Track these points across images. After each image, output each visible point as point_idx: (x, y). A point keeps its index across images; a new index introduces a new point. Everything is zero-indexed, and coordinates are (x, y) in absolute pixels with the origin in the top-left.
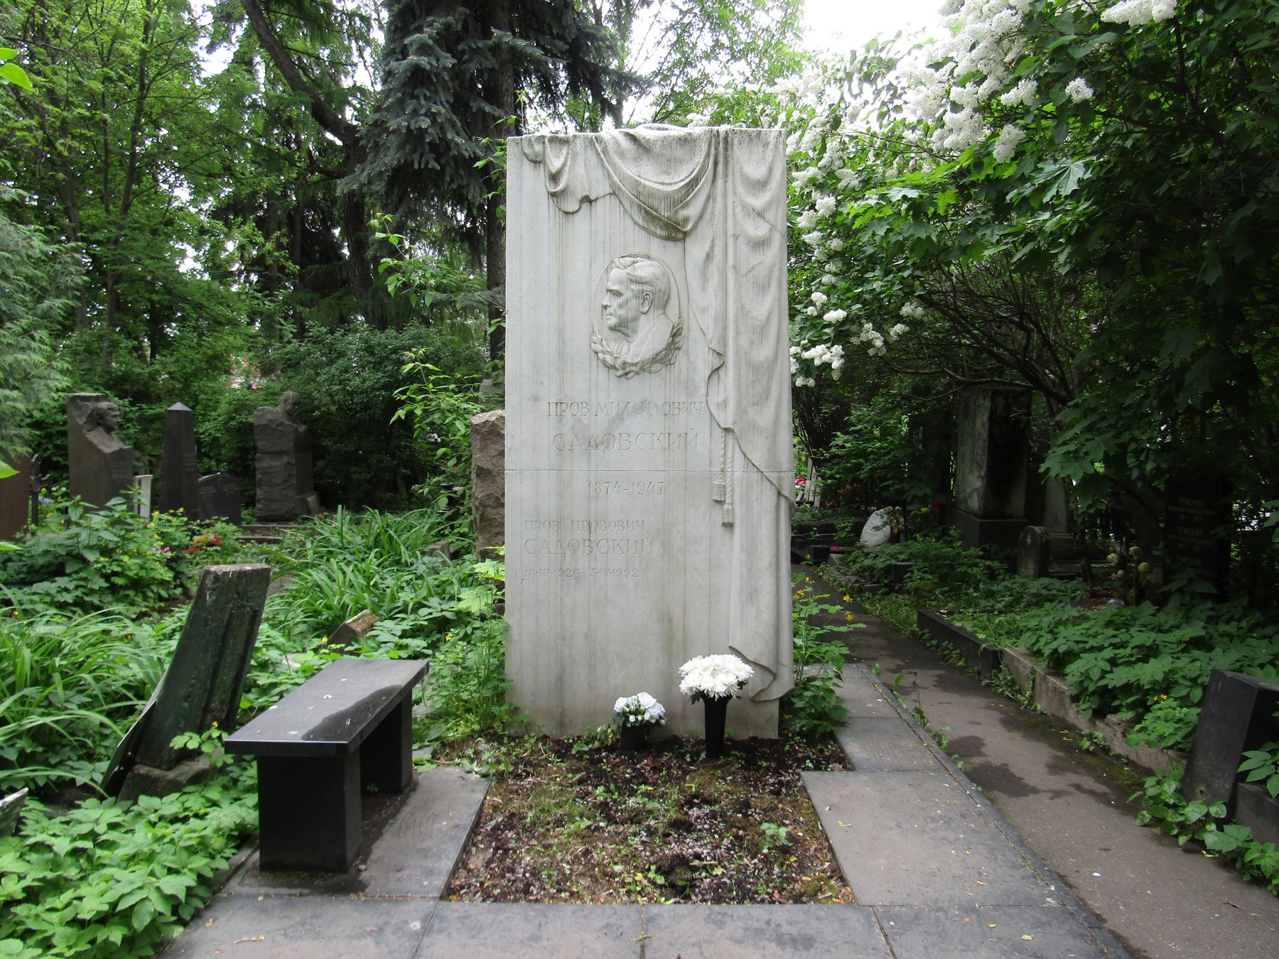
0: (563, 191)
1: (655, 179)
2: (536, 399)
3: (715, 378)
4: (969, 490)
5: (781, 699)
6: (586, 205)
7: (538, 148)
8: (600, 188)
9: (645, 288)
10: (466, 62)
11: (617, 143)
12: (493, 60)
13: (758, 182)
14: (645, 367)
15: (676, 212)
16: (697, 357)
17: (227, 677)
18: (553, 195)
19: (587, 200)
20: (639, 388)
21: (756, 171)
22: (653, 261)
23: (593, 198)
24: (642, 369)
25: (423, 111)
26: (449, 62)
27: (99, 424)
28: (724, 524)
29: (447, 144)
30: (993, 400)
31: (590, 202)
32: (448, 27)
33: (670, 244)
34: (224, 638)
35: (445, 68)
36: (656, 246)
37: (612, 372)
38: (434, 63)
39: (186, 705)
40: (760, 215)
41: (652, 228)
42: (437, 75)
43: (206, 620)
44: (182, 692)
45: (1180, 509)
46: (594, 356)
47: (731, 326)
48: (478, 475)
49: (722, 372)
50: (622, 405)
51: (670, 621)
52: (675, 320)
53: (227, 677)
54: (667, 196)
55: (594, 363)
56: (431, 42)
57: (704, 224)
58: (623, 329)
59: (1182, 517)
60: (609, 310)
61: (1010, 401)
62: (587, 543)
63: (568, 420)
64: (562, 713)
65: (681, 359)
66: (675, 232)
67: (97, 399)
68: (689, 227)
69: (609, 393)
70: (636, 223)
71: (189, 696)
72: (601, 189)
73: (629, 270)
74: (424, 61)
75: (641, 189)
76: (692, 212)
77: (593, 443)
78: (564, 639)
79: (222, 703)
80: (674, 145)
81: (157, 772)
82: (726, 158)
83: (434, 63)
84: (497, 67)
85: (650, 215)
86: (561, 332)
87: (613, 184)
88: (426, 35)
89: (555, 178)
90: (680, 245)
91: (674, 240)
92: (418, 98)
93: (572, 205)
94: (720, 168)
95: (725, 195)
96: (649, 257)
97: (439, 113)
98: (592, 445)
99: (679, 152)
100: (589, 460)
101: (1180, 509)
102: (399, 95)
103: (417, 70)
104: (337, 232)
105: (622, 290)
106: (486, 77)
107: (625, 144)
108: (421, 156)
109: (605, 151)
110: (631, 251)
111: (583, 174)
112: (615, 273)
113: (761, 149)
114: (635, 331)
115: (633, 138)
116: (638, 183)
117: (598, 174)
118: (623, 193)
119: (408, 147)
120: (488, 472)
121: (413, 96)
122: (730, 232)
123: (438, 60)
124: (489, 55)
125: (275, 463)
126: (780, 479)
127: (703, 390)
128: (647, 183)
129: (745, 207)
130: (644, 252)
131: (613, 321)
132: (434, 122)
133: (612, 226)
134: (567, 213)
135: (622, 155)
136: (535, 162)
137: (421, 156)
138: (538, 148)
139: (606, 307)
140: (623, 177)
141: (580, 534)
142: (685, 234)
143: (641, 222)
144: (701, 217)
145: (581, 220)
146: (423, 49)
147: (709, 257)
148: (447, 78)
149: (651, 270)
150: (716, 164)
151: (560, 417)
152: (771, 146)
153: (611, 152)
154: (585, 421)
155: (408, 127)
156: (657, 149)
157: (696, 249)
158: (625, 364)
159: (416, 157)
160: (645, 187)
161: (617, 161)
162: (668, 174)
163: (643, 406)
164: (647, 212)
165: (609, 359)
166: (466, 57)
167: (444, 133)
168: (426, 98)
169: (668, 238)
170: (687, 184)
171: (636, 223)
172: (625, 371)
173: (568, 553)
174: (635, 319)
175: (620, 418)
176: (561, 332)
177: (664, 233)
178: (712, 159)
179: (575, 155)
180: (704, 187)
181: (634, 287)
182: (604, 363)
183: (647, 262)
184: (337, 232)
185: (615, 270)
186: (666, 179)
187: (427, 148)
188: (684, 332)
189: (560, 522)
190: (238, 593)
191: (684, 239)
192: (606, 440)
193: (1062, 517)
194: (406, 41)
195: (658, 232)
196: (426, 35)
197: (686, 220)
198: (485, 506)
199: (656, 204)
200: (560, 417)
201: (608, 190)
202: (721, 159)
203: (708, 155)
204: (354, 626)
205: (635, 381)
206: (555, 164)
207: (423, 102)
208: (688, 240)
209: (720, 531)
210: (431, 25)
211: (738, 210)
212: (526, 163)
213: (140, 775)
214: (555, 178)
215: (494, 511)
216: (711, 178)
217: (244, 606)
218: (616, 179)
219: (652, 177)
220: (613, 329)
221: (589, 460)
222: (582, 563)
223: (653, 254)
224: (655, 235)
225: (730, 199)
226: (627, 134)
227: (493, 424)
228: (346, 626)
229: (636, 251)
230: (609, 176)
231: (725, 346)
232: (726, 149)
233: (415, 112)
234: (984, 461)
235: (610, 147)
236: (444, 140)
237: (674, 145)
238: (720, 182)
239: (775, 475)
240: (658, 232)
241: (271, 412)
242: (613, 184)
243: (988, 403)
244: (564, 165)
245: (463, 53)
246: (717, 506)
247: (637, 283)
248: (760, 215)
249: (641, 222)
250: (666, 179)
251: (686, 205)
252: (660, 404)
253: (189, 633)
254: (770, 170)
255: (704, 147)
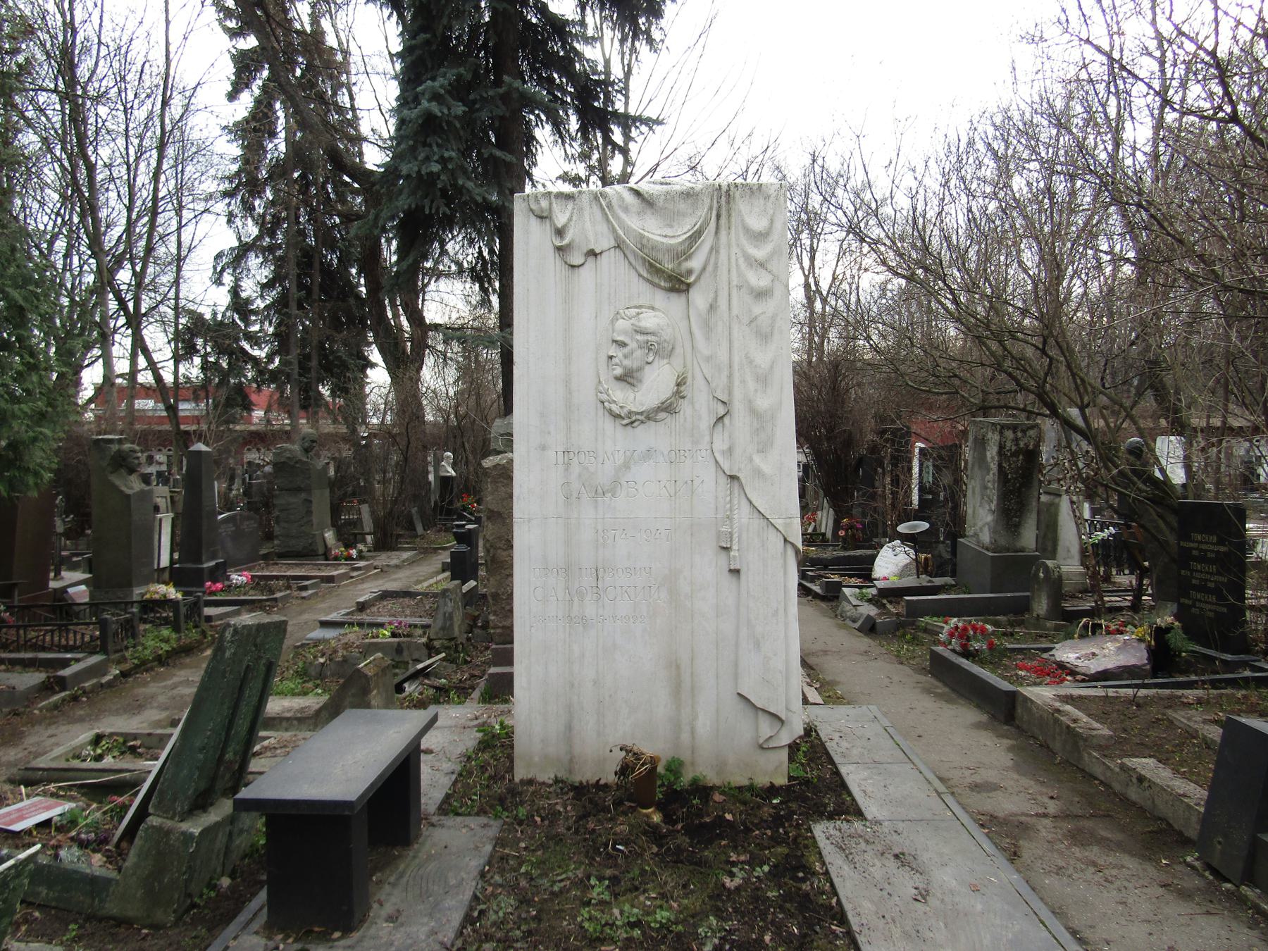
0: (569, 246)
1: (659, 232)
2: (543, 448)
3: (720, 425)
4: (980, 524)
5: (790, 746)
6: (591, 259)
7: (544, 204)
8: (603, 242)
9: (650, 338)
10: (478, 110)
11: (622, 199)
12: (504, 108)
13: (761, 234)
14: (649, 416)
15: (680, 264)
16: (699, 407)
17: (242, 725)
18: (559, 249)
19: (592, 254)
20: (646, 436)
21: (757, 223)
22: (662, 313)
23: (598, 251)
24: (648, 418)
25: (436, 158)
26: (459, 109)
27: (121, 466)
28: (731, 571)
29: (460, 190)
30: (1001, 433)
31: (595, 255)
32: (459, 76)
33: (674, 296)
34: (241, 689)
35: (456, 117)
36: (660, 298)
37: (618, 421)
38: (446, 111)
39: (201, 756)
40: (762, 265)
41: (657, 281)
42: (448, 123)
43: (225, 671)
44: (198, 743)
45: (1192, 545)
46: (600, 405)
47: (736, 375)
48: (489, 518)
49: (726, 420)
50: (628, 453)
51: (678, 667)
52: (680, 369)
53: (242, 725)
54: (669, 249)
55: (601, 412)
56: (442, 91)
57: (707, 274)
58: (628, 378)
59: (1195, 553)
60: (615, 360)
61: (1019, 434)
62: (595, 590)
63: (576, 469)
64: (571, 761)
65: (685, 407)
66: (678, 284)
67: (120, 441)
68: (692, 279)
69: (617, 441)
70: (640, 275)
71: (204, 748)
72: (603, 242)
73: (633, 321)
74: (435, 108)
75: (645, 241)
76: (695, 263)
77: (600, 491)
78: (573, 685)
79: (235, 754)
80: (677, 199)
81: (169, 823)
82: (729, 210)
83: (446, 111)
84: (507, 115)
85: (654, 269)
86: (567, 382)
87: (617, 237)
88: (439, 84)
89: (560, 232)
90: (683, 296)
91: (678, 291)
92: (430, 146)
93: (577, 259)
94: (723, 220)
95: (729, 246)
96: (653, 308)
97: (451, 159)
98: (599, 492)
99: (682, 206)
100: (596, 507)
101: (1192, 545)
102: (411, 143)
103: (429, 118)
104: (354, 271)
105: (627, 340)
106: (497, 124)
107: (629, 198)
108: (432, 202)
109: (610, 206)
110: (635, 303)
111: (589, 229)
112: (621, 324)
113: (762, 201)
114: (640, 381)
115: (637, 193)
116: (642, 236)
117: (603, 228)
118: (628, 246)
119: (420, 193)
120: (499, 514)
121: (425, 144)
122: (734, 283)
123: (449, 109)
124: (499, 103)
125: (292, 500)
126: (786, 525)
127: (707, 438)
128: (651, 236)
129: (747, 257)
130: (648, 304)
131: (619, 371)
132: (445, 168)
133: (615, 278)
134: (573, 266)
135: (626, 209)
136: (542, 218)
137: (432, 202)
138: (544, 204)
139: (611, 357)
140: (627, 230)
141: (588, 580)
142: (689, 285)
143: (645, 275)
144: (704, 269)
145: (587, 273)
146: (436, 97)
147: (712, 307)
148: (458, 126)
149: (657, 320)
150: (718, 217)
151: (568, 465)
152: (772, 199)
153: (616, 208)
154: (592, 469)
155: (419, 172)
156: (661, 203)
157: (699, 298)
158: (630, 412)
159: (427, 202)
160: (648, 240)
161: (623, 216)
162: (671, 226)
163: (649, 454)
164: (651, 264)
165: (615, 408)
166: (477, 106)
167: (455, 179)
168: (438, 145)
169: (672, 290)
170: (690, 237)
171: (640, 275)
172: (631, 420)
173: (576, 599)
174: (640, 369)
175: (627, 466)
176: (567, 382)
177: (667, 285)
178: (714, 213)
179: (581, 209)
180: (707, 240)
181: (639, 337)
182: (610, 412)
183: (651, 313)
184: (354, 271)
185: (621, 321)
186: (669, 232)
187: (439, 194)
188: (689, 381)
189: (568, 570)
190: (256, 646)
191: (687, 291)
192: (612, 489)
193: (1075, 550)
194: (419, 89)
195: (662, 284)
196: (439, 84)
197: (690, 272)
198: (496, 549)
199: (660, 256)
200: (568, 465)
201: (613, 243)
202: (724, 213)
203: (711, 208)
204: (366, 671)
205: (640, 430)
206: (561, 219)
207: (435, 149)
208: (691, 291)
209: (727, 579)
210: (444, 76)
211: (741, 261)
212: (533, 219)
213: (153, 827)
214: (560, 232)
215: (504, 553)
216: (713, 230)
217: (260, 657)
218: (620, 232)
219: (654, 230)
220: (619, 379)
221: (596, 507)
222: (590, 611)
223: (657, 305)
224: (659, 286)
225: (734, 250)
226: (631, 189)
227: (504, 467)
228: (359, 670)
229: (641, 303)
230: (614, 231)
231: (730, 394)
232: (728, 202)
233: (427, 159)
234: (993, 493)
235: (614, 202)
236: (454, 186)
237: (677, 199)
238: (723, 233)
239: (780, 521)
240: (662, 284)
241: (290, 450)
242: (617, 237)
243: (997, 437)
244: (570, 219)
245: (474, 102)
246: (724, 553)
247: (642, 333)
248: (762, 265)
249: (645, 275)
250: (669, 232)
251: (689, 257)
252: (666, 453)
253: (211, 675)
254: (772, 221)
255: (707, 201)
